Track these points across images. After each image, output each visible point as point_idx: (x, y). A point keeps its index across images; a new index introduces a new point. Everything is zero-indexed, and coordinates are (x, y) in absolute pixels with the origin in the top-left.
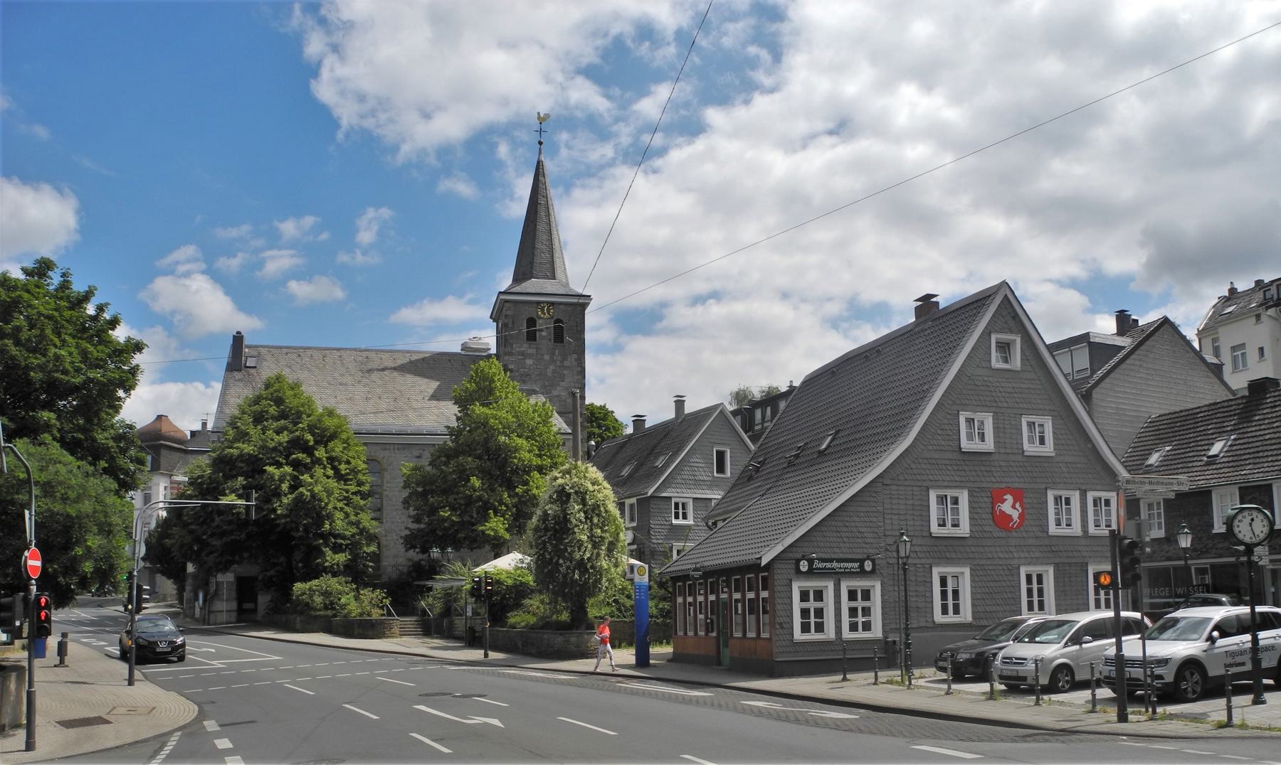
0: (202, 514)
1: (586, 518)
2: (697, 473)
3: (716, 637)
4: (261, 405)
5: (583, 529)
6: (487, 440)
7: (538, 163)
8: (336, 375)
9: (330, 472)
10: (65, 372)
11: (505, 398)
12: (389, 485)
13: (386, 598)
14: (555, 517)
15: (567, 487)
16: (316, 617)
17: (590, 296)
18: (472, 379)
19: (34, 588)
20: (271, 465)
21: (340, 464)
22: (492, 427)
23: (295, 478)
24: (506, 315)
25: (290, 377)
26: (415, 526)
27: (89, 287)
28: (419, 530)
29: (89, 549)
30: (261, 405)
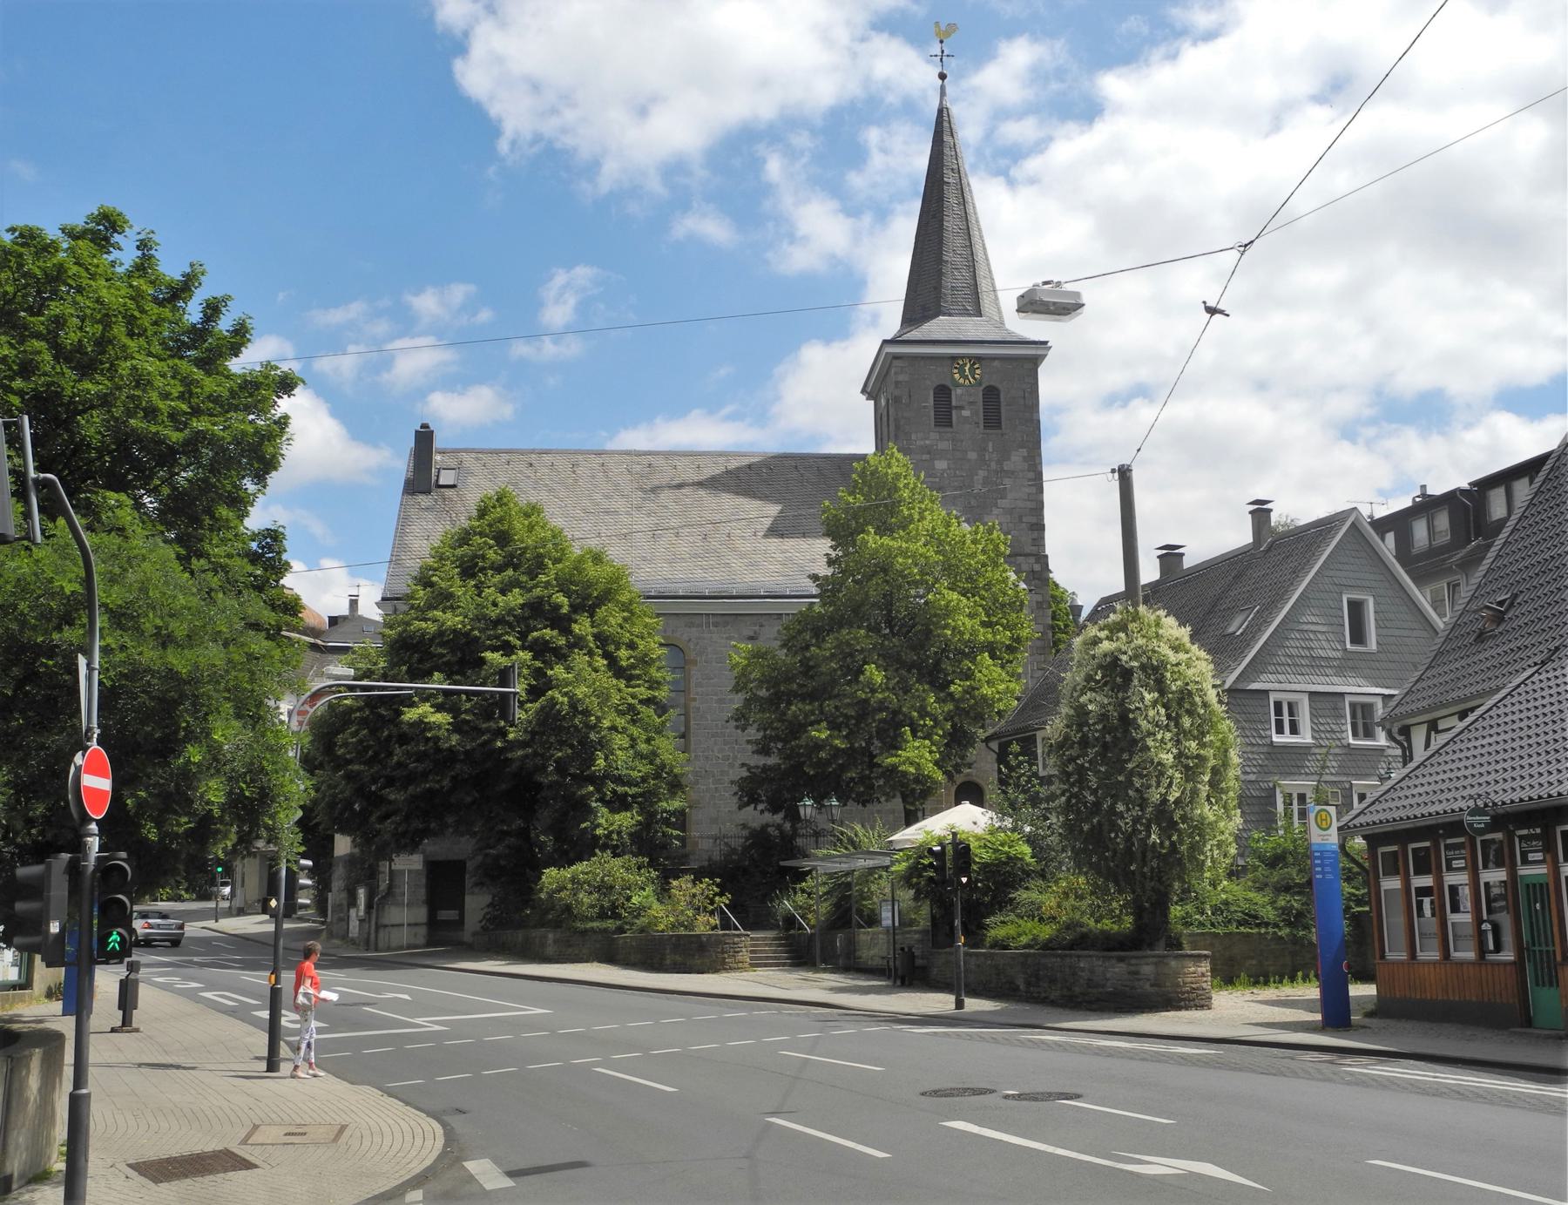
0: (371, 743)
1: (1169, 717)
2: (1315, 644)
3: (1513, 963)
4: (471, 545)
5: (1162, 741)
6: (888, 602)
7: (940, 111)
8: (598, 497)
9: (601, 662)
10: (151, 413)
11: (919, 521)
12: (700, 689)
13: (721, 894)
14: (1103, 717)
15: (1124, 658)
16: (585, 932)
17: (1046, 343)
18: (855, 487)
19: (94, 843)
20: (494, 649)
21: (618, 649)
22: (901, 574)
23: (538, 673)
24: (897, 383)
25: (526, 496)
26: (761, 761)
27: (192, 265)
28: (765, 769)
29: (214, 752)
30: (471, 545)
